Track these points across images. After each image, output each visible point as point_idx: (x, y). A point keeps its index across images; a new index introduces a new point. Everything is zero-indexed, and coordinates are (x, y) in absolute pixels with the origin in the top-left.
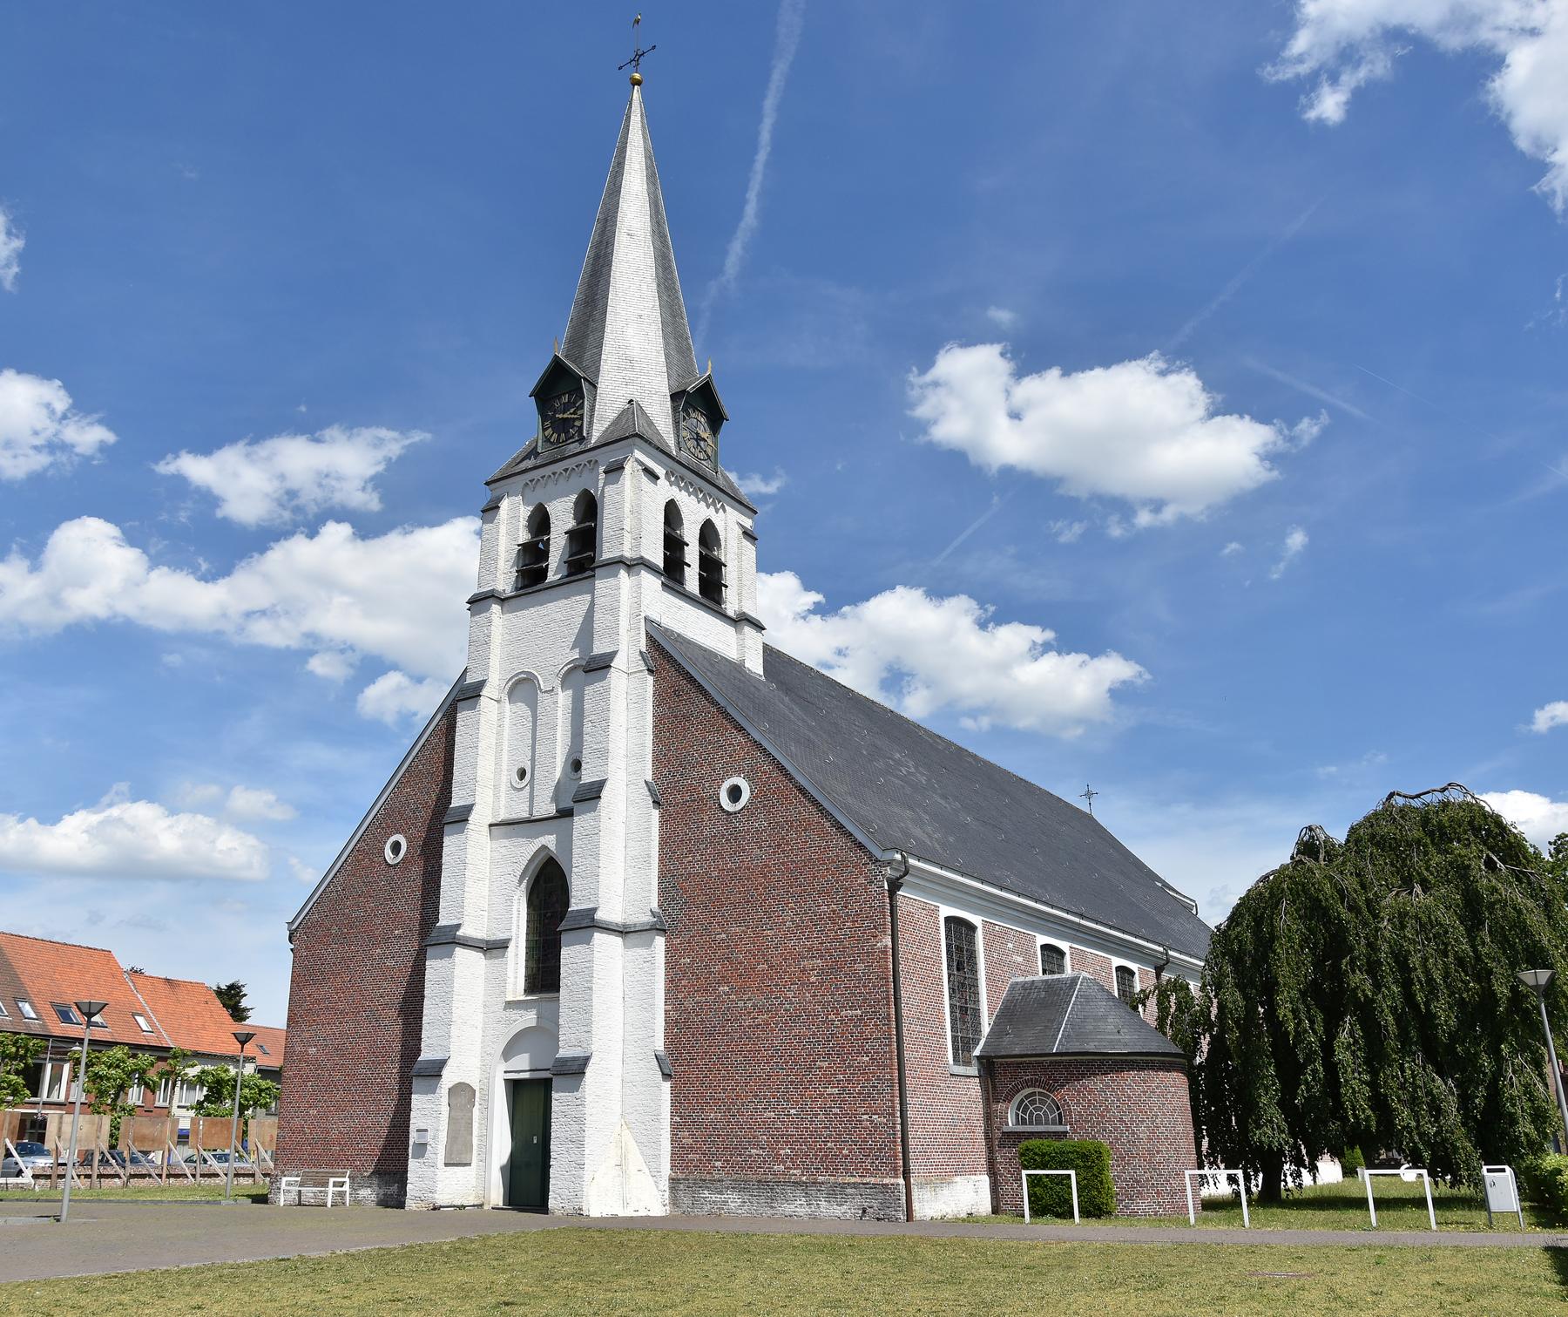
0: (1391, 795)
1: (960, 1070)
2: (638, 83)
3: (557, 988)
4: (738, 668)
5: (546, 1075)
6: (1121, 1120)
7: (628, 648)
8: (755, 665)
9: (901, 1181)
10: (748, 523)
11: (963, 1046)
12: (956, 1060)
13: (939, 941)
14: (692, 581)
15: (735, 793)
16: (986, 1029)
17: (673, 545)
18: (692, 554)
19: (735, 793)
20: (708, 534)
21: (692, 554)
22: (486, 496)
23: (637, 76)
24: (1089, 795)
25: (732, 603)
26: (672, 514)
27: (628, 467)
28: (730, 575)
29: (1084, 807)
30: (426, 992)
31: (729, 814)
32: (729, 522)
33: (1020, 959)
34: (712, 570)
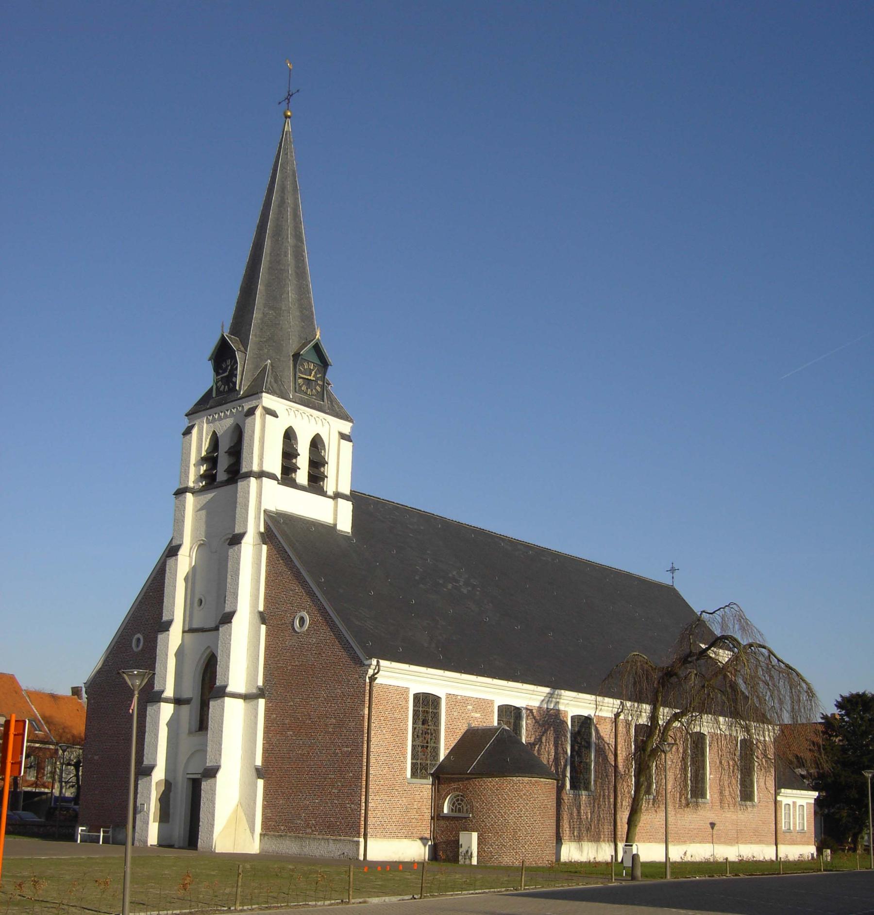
0: (702, 612)
1: (415, 780)
2: (289, 117)
3: (207, 729)
4: (332, 529)
5: (199, 776)
6: (499, 812)
7: (253, 527)
8: (345, 525)
9: (362, 840)
10: (346, 427)
11: (417, 771)
12: (414, 774)
13: (407, 708)
14: (302, 476)
15: (302, 620)
16: (442, 757)
17: (289, 455)
18: (303, 462)
19: (302, 620)
20: (316, 444)
21: (303, 462)
22: (186, 423)
23: (289, 114)
24: (673, 570)
25: (330, 486)
26: (289, 436)
27: (259, 412)
28: (330, 470)
29: (665, 579)
30: (147, 729)
31: (296, 632)
32: (331, 428)
33: (478, 715)
34: (317, 464)
